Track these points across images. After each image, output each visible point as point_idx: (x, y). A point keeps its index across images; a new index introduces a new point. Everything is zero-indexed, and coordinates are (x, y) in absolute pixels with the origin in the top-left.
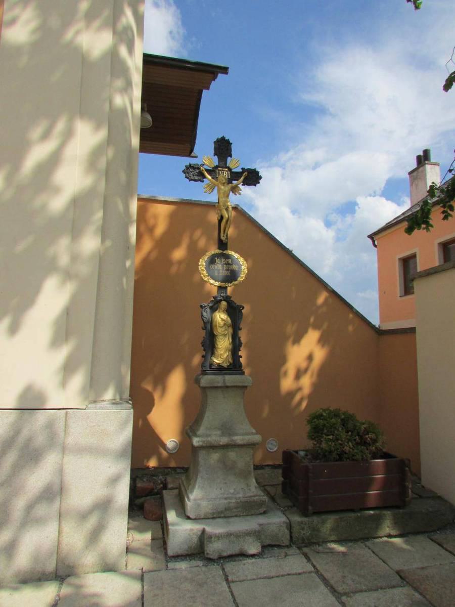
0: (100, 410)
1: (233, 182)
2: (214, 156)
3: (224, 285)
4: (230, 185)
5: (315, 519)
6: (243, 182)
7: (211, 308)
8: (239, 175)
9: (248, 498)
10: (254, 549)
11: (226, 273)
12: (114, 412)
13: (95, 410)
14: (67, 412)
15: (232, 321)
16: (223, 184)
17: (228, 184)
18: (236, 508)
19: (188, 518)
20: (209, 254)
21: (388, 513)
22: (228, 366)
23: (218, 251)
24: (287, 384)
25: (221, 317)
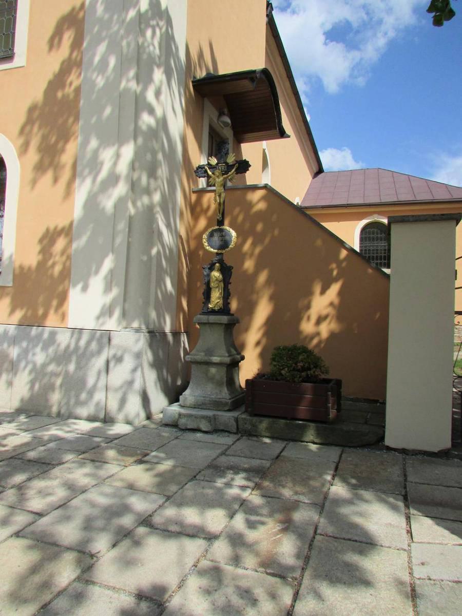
3: (220, 251)
5: (255, 419)
7: (209, 269)
10: (204, 426)
11: (221, 243)
15: (223, 276)
16: (218, 177)
18: (210, 404)
21: (312, 425)
22: (218, 310)
23: (217, 227)
24: (307, 327)
25: (216, 274)
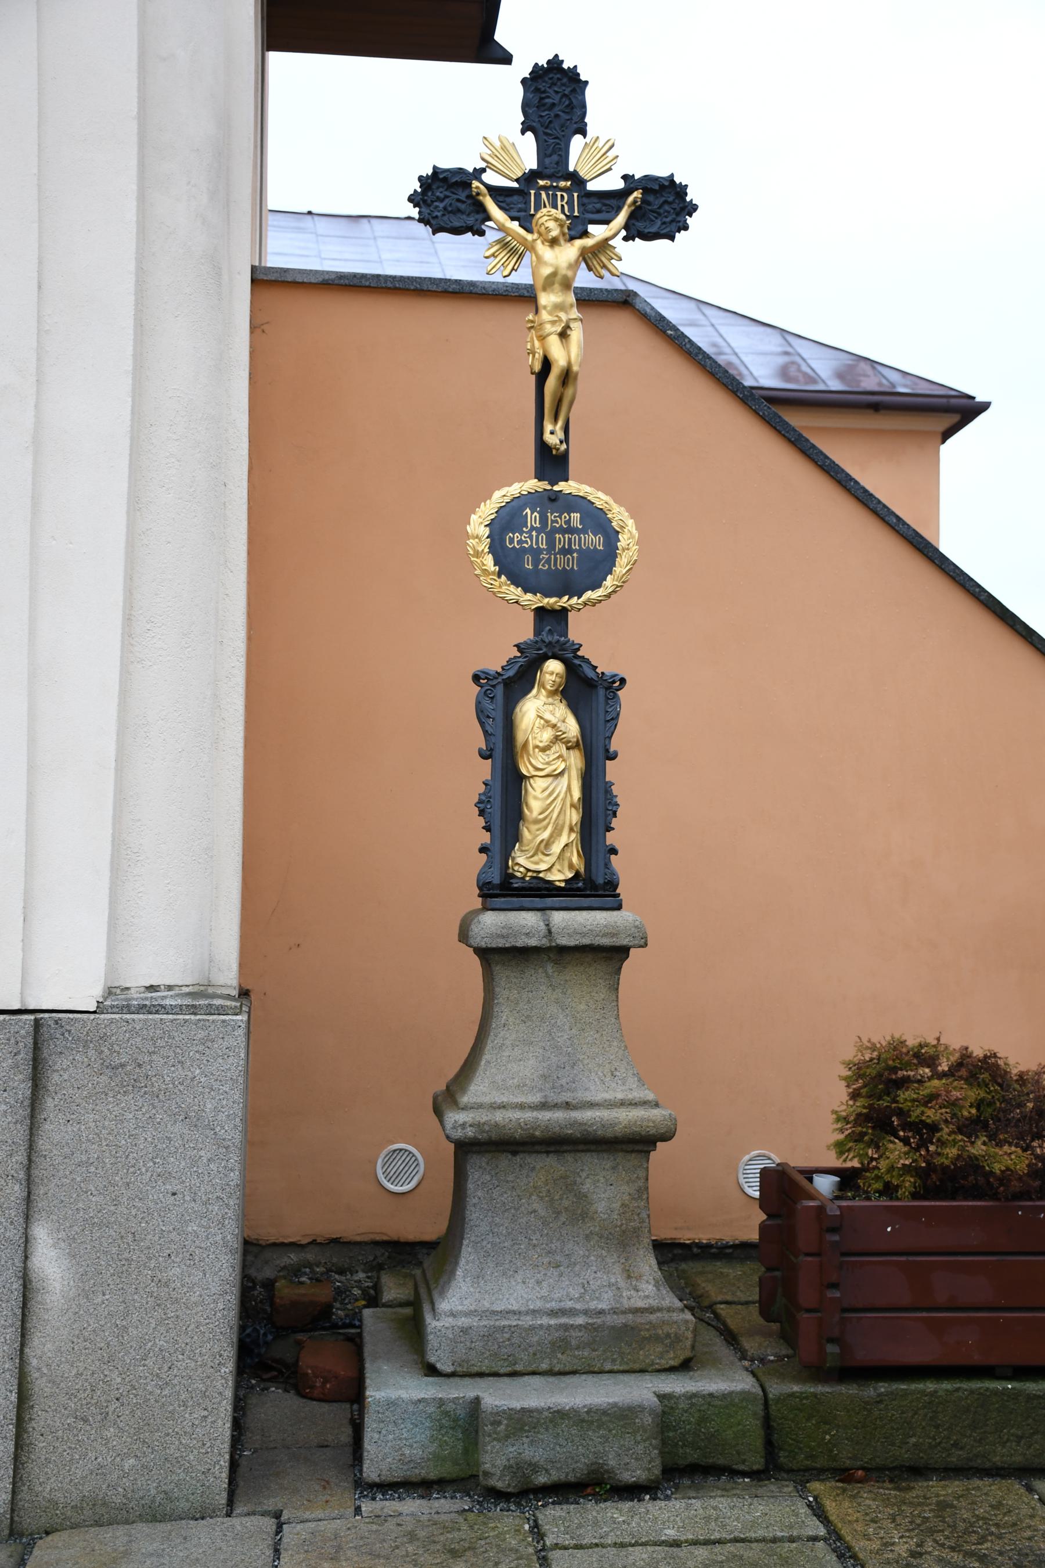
0: (141, 1016)
1: (591, 228)
2: (523, 132)
4: (579, 243)
6: (626, 227)
8: (613, 202)
9: (630, 1316)
12: (186, 1021)
13: (128, 1016)
14: (36, 1020)
17: (572, 238)
19: (431, 1370)
20: (500, 496)
23: (533, 485)
